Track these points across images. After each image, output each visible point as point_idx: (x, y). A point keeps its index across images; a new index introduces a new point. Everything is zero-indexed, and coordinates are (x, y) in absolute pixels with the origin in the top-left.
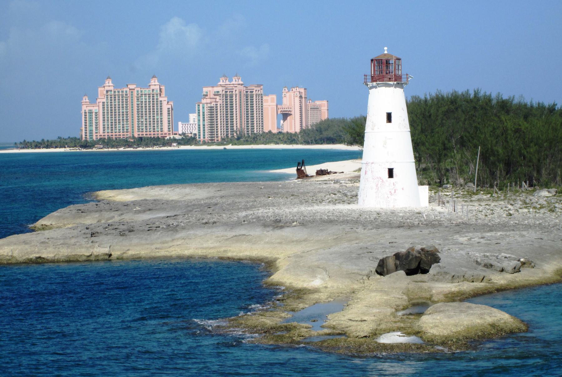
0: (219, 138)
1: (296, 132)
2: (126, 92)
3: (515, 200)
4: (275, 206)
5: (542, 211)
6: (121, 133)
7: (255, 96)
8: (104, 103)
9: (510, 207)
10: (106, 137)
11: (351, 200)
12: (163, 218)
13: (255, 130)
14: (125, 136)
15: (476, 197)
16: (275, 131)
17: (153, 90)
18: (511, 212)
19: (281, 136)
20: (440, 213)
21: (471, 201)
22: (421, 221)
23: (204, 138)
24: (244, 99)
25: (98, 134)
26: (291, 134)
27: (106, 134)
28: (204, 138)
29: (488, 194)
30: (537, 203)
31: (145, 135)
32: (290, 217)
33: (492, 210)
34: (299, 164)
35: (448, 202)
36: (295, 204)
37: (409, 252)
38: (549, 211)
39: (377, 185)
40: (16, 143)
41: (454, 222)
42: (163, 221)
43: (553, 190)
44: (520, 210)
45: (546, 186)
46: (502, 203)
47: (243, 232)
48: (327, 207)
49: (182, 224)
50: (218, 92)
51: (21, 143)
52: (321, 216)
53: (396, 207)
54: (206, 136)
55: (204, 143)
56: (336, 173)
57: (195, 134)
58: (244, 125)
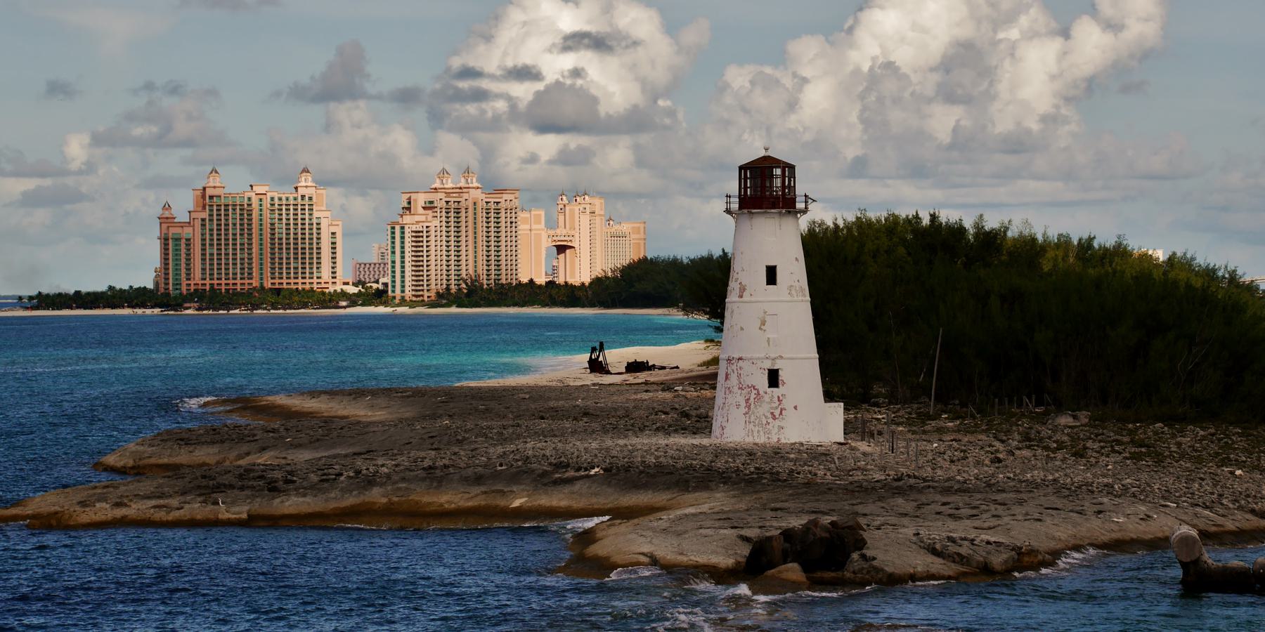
0: (433, 294)
1: (583, 284)
2: (249, 199)
3: (1008, 432)
4: (555, 436)
5: (1059, 455)
6: (238, 281)
7: (503, 211)
8: (203, 220)
9: (997, 444)
10: (208, 288)
11: (698, 425)
12: (346, 456)
13: (503, 277)
14: (246, 287)
15: (933, 423)
16: (541, 280)
17: (303, 197)
18: (1001, 456)
19: (554, 292)
20: (864, 454)
21: (924, 432)
22: (829, 470)
23: (403, 291)
24: (481, 216)
25: (192, 282)
26: (573, 287)
27: (208, 282)
28: (403, 291)
29: (957, 418)
30: (1050, 438)
31: (285, 286)
32: (586, 457)
33: (964, 451)
34: (594, 350)
35: (880, 433)
36: (593, 432)
37: (808, 529)
38: (1074, 455)
39: (747, 400)
40: (20, 298)
41: (892, 473)
42: (348, 461)
43: (1084, 417)
44: (1017, 452)
45: (1074, 407)
46: (983, 437)
47: (499, 487)
48: (654, 440)
49: (385, 470)
50: (431, 202)
51: (31, 298)
52: (642, 457)
53: (783, 441)
54: (407, 289)
55: (403, 302)
56: (663, 368)
57: (386, 285)
58: (482, 269)
